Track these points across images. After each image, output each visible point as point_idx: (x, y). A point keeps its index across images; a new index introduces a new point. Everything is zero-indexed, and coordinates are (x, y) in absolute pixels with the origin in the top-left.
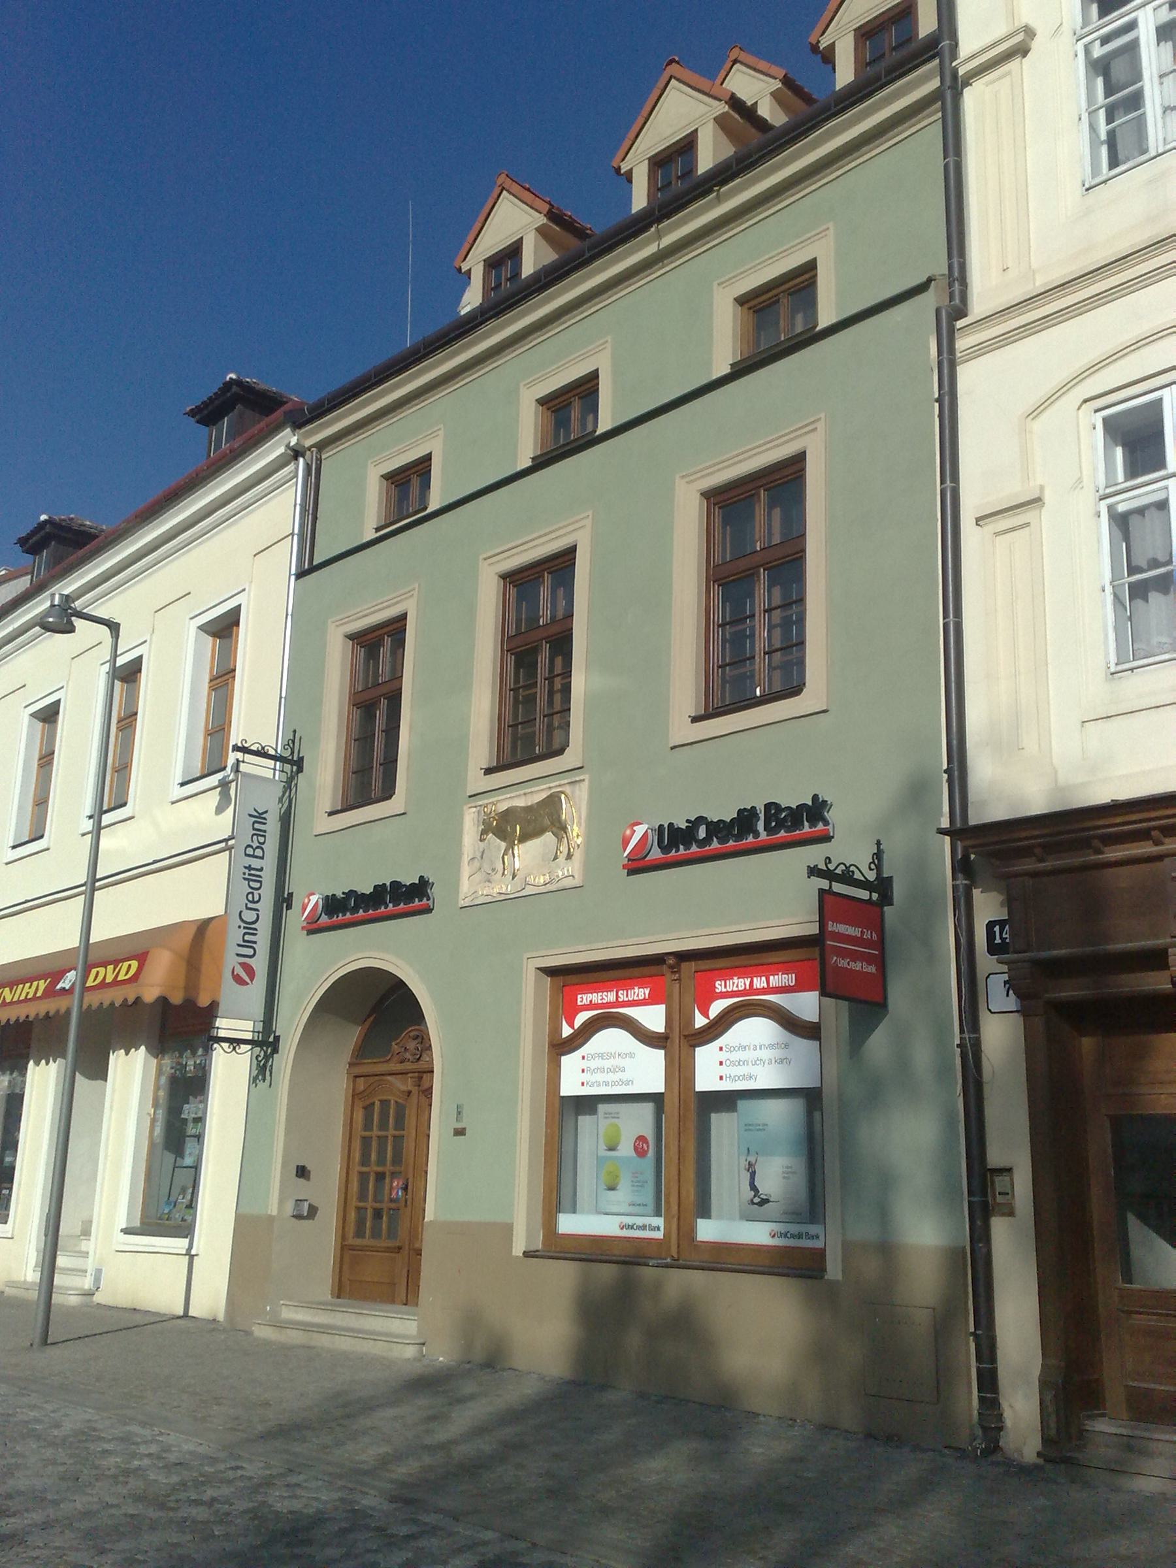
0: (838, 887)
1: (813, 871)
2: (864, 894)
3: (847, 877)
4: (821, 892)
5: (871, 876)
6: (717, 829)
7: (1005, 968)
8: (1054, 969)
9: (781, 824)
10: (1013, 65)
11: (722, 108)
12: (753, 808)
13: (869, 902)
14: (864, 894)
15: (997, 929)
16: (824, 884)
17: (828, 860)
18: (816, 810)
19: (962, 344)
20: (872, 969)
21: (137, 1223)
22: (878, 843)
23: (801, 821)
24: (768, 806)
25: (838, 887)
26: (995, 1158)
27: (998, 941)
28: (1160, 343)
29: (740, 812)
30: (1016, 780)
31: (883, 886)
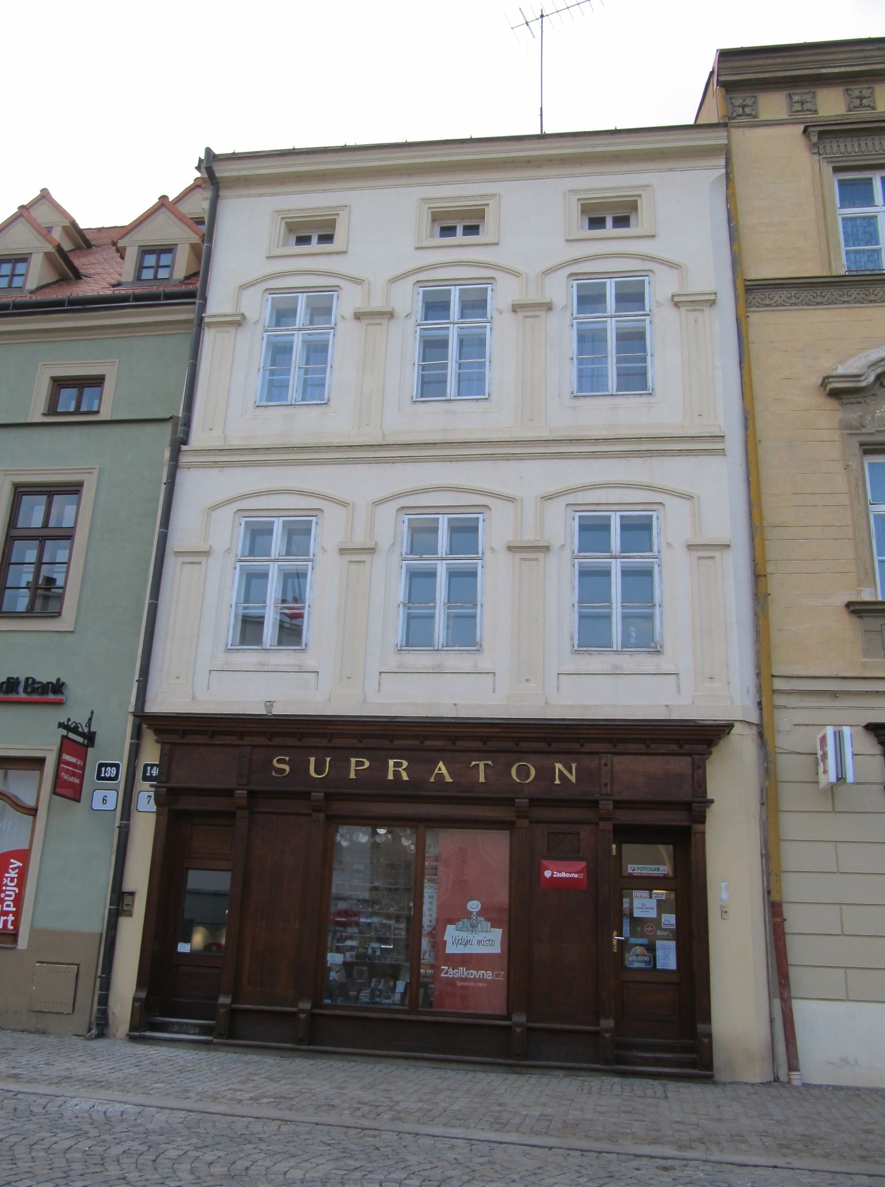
0: (71, 735)
1: (61, 725)
2: (80, 739)
3: (75, 730)
4: (63, 737)
5: (86, 730)
6: (32, 686)
7: (153, 789)
8: (172, 791)
9: (34, 691)
10: (232, 330)
11: (50, 249)
12: (18, 678)
13: (82, 744)
14: (80, 739)
15: (149, 768)
16: (64, 732)
17: (69, 720)
18: (58, 687)
19: (184, 459)
20: (77, 781)
21: (48, 411)
22: (92, 713)
23: (50, 692)
24: (27, 679)
25: (71, 735)
26: (128, 886)
27: (148, 774)
28: (398, 467)
29: (9, 679)
30: (177, 692)
31: (90, 738)
